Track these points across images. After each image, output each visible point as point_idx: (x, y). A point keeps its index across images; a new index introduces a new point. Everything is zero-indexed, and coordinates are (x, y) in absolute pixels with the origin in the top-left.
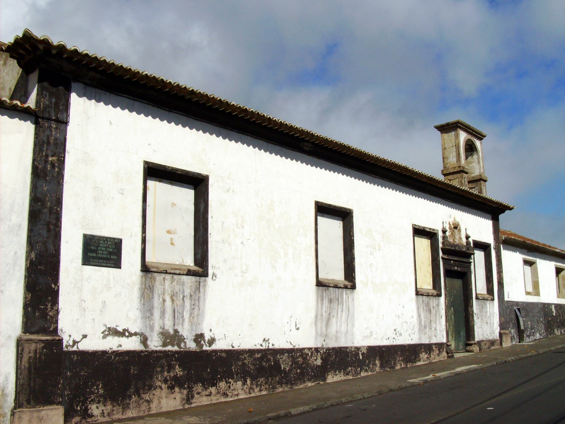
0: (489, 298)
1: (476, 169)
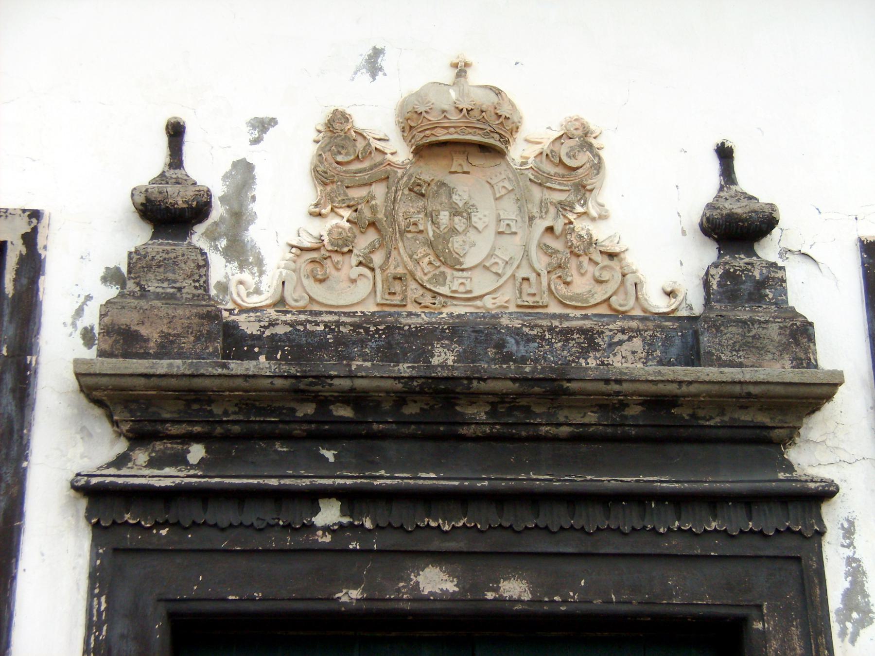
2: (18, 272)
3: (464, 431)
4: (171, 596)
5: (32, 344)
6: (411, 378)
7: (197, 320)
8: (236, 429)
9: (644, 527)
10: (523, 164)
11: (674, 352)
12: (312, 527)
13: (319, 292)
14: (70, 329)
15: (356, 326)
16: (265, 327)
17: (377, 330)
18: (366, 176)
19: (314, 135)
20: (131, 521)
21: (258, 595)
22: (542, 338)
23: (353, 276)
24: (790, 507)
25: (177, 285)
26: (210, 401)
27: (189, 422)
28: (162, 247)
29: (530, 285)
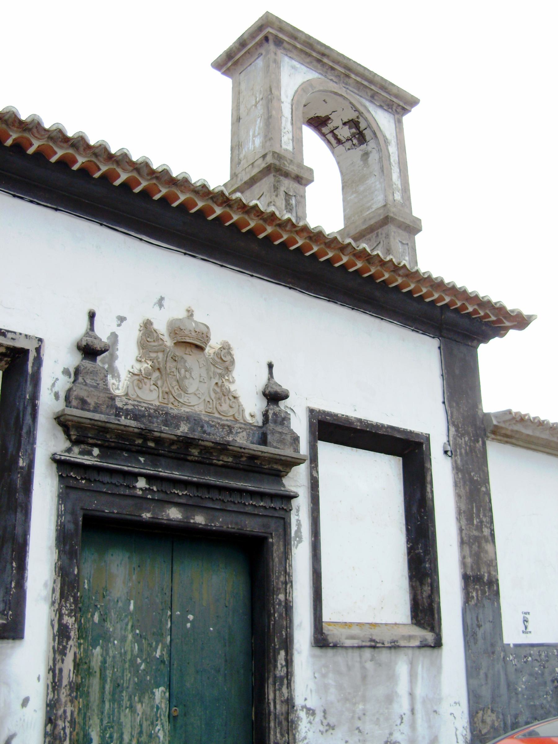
0: (410, 638)
1: (376, 193)
2: (33, 364)
3: (189, 458)
4: (85, 508)
5: (38, 396)
6: (181, 436)
7: (107, 399)
8: (113, 444)
9: (242, 502)
10: (209, 356)
11: (256, 439)
12: (135, 487)
13: (139, 392)
14: (50, 391)
15: (155, 410)
16: (125, 405)
17: (162, 413)
18: (156, 348)
19: (139, 327)
20: (74, 476)
21: (115, 511)
22: (216, 426)
23: (152, 389)
24: (284, 500)
25: (97, 382)
26: (107, 432)
27: (97, 439)
28: (88, 364)
29: (210, 404)
